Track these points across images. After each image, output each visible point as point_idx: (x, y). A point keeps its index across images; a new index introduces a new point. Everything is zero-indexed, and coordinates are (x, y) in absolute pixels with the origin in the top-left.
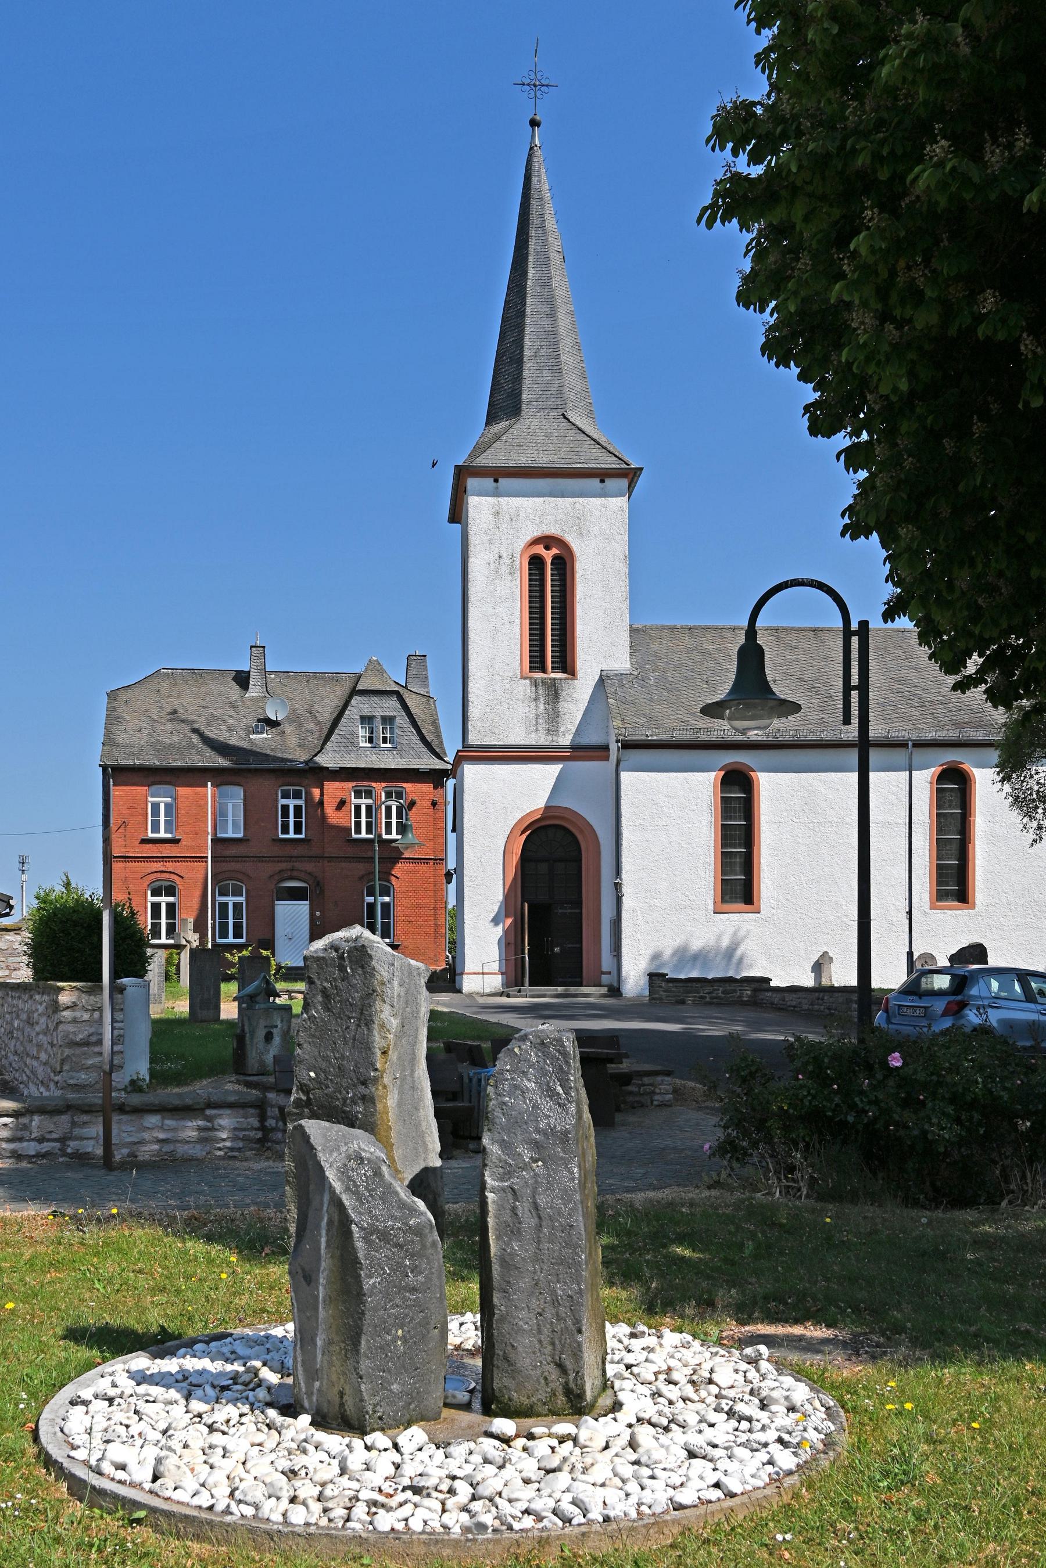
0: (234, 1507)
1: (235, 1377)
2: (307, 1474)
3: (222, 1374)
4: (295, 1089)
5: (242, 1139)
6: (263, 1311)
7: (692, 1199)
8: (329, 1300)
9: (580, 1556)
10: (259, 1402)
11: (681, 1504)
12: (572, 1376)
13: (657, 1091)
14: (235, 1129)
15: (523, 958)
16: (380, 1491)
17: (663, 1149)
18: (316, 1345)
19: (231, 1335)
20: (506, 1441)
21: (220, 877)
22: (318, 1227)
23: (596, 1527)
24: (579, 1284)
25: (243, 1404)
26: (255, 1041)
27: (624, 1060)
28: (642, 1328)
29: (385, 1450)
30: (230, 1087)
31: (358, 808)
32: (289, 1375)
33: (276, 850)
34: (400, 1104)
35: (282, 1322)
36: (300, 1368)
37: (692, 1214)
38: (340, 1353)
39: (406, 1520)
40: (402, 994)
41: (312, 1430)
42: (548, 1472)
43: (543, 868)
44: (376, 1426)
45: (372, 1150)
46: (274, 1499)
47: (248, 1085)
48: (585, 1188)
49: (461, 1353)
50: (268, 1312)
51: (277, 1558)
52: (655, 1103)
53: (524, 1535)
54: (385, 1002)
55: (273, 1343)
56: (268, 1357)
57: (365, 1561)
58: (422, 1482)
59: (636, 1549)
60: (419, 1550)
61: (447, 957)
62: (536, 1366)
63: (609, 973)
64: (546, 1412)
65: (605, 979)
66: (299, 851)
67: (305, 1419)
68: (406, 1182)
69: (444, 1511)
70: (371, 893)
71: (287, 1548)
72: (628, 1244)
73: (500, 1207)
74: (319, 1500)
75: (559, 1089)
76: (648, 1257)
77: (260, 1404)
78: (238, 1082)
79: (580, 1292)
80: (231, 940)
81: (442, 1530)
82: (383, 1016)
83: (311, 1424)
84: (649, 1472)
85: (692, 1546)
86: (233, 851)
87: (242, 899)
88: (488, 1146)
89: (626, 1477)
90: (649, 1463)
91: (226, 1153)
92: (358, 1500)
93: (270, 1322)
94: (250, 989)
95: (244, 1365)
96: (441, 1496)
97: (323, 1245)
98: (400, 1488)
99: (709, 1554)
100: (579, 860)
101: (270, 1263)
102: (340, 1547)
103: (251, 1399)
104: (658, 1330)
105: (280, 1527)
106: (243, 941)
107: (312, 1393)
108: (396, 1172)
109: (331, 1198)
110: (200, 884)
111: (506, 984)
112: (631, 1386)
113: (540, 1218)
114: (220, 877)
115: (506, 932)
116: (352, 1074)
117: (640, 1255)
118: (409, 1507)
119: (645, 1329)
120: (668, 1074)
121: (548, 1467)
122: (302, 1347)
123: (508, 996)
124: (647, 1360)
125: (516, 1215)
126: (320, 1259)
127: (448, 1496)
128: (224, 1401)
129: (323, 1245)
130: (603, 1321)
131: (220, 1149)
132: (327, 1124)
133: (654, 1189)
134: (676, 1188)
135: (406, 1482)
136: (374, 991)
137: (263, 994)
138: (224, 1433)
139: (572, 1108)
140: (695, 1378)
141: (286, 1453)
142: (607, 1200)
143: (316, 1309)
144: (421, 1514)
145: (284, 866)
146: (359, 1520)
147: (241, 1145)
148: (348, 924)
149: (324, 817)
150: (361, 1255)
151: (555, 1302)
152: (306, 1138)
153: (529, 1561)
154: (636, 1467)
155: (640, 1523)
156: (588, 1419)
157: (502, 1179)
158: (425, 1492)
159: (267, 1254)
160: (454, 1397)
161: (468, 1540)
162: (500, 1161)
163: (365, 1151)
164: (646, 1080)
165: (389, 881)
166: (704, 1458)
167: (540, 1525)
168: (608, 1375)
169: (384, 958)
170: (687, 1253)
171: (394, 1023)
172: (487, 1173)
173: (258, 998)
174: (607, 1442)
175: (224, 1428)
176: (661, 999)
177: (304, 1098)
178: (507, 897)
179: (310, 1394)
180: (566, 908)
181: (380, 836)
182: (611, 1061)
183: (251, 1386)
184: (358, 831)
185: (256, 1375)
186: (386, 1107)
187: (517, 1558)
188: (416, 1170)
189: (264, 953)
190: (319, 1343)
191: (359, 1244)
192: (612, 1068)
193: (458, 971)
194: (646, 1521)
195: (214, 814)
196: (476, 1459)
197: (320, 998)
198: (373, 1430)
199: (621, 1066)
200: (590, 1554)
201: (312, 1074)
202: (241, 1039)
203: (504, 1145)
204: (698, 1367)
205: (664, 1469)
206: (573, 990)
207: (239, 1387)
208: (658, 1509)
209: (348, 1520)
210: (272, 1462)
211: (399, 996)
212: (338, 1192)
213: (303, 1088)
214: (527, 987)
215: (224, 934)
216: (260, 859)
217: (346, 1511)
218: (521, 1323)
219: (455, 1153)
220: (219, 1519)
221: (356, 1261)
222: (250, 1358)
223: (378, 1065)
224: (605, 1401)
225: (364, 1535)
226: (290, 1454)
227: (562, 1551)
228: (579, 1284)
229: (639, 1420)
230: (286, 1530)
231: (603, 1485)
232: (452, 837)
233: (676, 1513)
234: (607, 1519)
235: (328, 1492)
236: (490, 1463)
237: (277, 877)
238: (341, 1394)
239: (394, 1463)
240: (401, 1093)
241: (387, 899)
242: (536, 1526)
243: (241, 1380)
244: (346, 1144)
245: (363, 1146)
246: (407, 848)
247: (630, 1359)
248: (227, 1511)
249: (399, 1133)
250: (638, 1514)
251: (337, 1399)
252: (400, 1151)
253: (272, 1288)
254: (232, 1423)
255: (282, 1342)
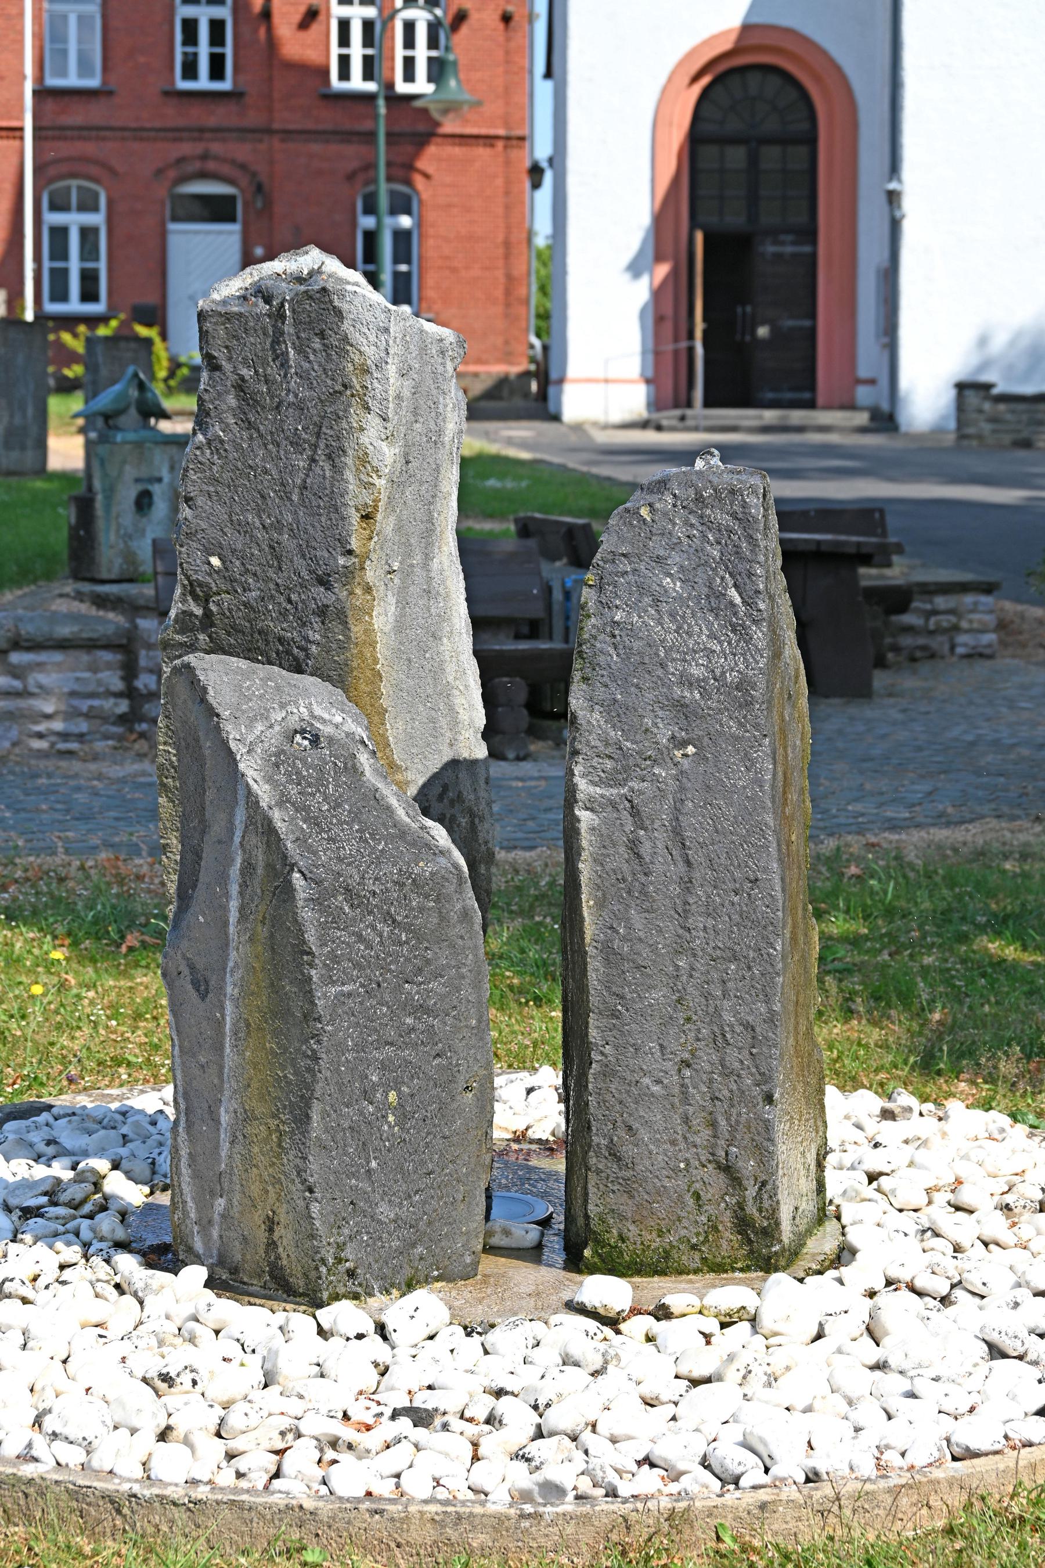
0: (41, 1449)
1: (53, 1191)
2: (195, 1383)
3: (26, 1185)
4: (178, 591)
5: (88, 716)
6: (118, 1061)
7: (1027, 844)
8: (245, 1029)
9: (754, 1550)
10: (102, 1239)
11: (967, 1449)
12: (751, 1192)
13: (964, 625)
14: (73, 694)
15: (691, 350)
16: (346, 1416)
17: (973, 744)
18: (217, 1122)
19: (49, 1107)
20: (613, 1322)
21: (52, 171)
22: (223, 879)
23: (790, 1492)
24: (767, 1001)
25: (69, 1244)
26: (114, 510)
27: (895, 558)
28: (905, 1099)
29: (360, 1337)
30: (61, 606)
31: (344, 25)
32: (164, 1189)
33: (172, 115)
34: (400, 627)
35: (157, 1083)
36: (185, 1171)
37: (1026, 875)
38: (266, 1140)
39: (398, 1476)
40: (406, 393)
41: (209, 1295)
42: (695, 1383)
43: (737, 156)
44: (341, 1290)
45: (338, 719)
46: (124, 1432)
47: (101, 602)
48: (785, 803)
49: (525, 1146)
50: (129, 1064)
51: (130, 1553)
52: (960, 650)
53: (640, 1506)
54: (368, 409)
55: (137, 1124)
56: (124, 1152)
57: (310, 1557)
58: (425, 1401)
59: (871, 1537)
60: (421, 1535)
61: (532, 347)
62: (676, 1170)
63: (872, 382)
64: (698, 1264)
65: (863, 394)
66: (219, 116)
67: (195, 1274)
68: (412, 791)
69: (476, 1458)
70: (370, 209)
71: (150, 1530)
72: (888, 934)
73: (605, 841)
74: (219, 1435)
75: (733, 594)
76: (928, 960)
77: (103, 1245)
78: (79, 596)
79: (771, 1019)
80: (74, 306)
81: (470, 1495)
82: (364, 439)
83: (207, 1285)
84: (905, 1385)
85: (984, 1532)
86: (77, 116)
87: (97, 219)
88: (580, 714)
89: (853, 1395)
90: (905, 1365)
91: (53, 745)
92: (299, 1436)
93: (132, 1082)
94: (105, 399)
95: (74, 1168)
96: (471, 1429)
97: (233, 916)
98: (388, 1412)
99: (1023, 1546)
100: (811, 140)
101: (137, 965)
102: (258, 1527)
103: (86, 1234)
104: (938, 1104)
105: (136, 1488)
106: (97, 308)
107: (210, 1222)
108: (390, 769)
109: (249, 818)
110: (8, 187)
111: (655, 404)
112: (878, 1217)
113: (688, 863)
114: (52, 171)
115: (657, 294)
116: (298, 561)
117: (911, 956)
118: (404, 1450)
119: (912, 1101)
120: (989, 589)
121: (696, 1374)
122: (189, 1126)
123: (659, 428)
124: (911, 1164)
125: (638, 856)
126: (225, 945)
127: (487, 1428)
128: (28, 1238)
129: (233, 916)
130: (821, 1080)
131: (40, 736)
132: (243, 664)
133: (948, 824)
134: (994, 823)
135: (402, 1401)
136: (345, 386)
137: (133, 411)
138: (25, 1301)
139: (759, 635)
140: (1009, 1199)
141: (154, 1342)
142: (848, 845)
143: (219, 1048)
144: (428, 1465)
145: (187, 148)
146: (299, 1476)
147: (83, 726)
148: (296, 244)
149: (272, 43)
150: (311, 936)
151: (719, 1040)
152: (199, 692)
153: (648, 1558)
154: (878, 1373)
155: (882, 1484)
156: (780, 1282)
157: (612, 780)
158: (438, 1421)
159: (131, 949)
160: (507, 1233)
161: (523, 1516)
162: (607, 744)
163: (324, 721)
164: (941, 602)
165: (408, 182)
166: (1020, 1358)
167: (674, 1488)
168: (829, 1195)
169: (368, 316)
170: (1011, 952)
171: (388, 454)
172: (577, 770)
173: (123, 420)
174: (821, 1325)
175: (27, 1292)
176: (980, 437)
177: (198, 611)
178: (658, 219)
179: (205, 1224)
180: (783, 243)
181: (390, 86)
182: (866, 559)
183: (87, 1208)
184: (345, 74)
185: (97, 1186)
186: (369, 631)
187: (624, 1553)
188: (435, 764)
189: (143, 331)
190: (225, 1118)
191: (307, 914)
192: (869, 575)
193: (554, 375)
194: (894, 1481)
195: (38, 36)
196: (548, 1356)
197: (232, 400)
198: (336, 1297)
199: (887, 572)
200: (777, 1547)
201: (215, 561)
202: (85, 505)
203: (614, 711)
204: (1017, 1179)
205: (936, 1379)
206: (797, 416)
207: (61, 1211)
208: (919, 1457)
209: (277, 1475)
210: (124, 1360)
211: (398, 397)
212: (263, 804)
213: (196, 591)
214: (698, 410)
215: (60, 294)
216: (138, 133)
217: (275, 1458)
218: (646, 1081)
219: (532, 748)
220: (10, 1470)
221: (302, 950)
222: (86, 1154)
223: (354, 544)
224: (824, 1242)
225: (309, 1504)
226: (161, 1343)
227: (719, 1539)
228: (767, 1001)
229: (889, 1283)
230: (147, 1493)
231: (808, 1410)
232: (544, 90)
233: (958, 1464)
234: (812, 1477)
235: (235, 1420)
236: (577, 1364)
237: (172, 174)
238: (271, 1224)
239: (376, 1365)
240: (403, 603)
241: (405, 221)
242: (667, 1490)
243: (64, 1197)
244: (283, 706)
245: (318, 711)
246: (446, 111)
247: (875, 1161)
248: (28, 1457)
249: (398, 687)
250: (878, 1466)
251: (262, 1236)
252: (400, 725)
253: (138, 1016)
254: (41, 1282)
255: (154, 1123)
